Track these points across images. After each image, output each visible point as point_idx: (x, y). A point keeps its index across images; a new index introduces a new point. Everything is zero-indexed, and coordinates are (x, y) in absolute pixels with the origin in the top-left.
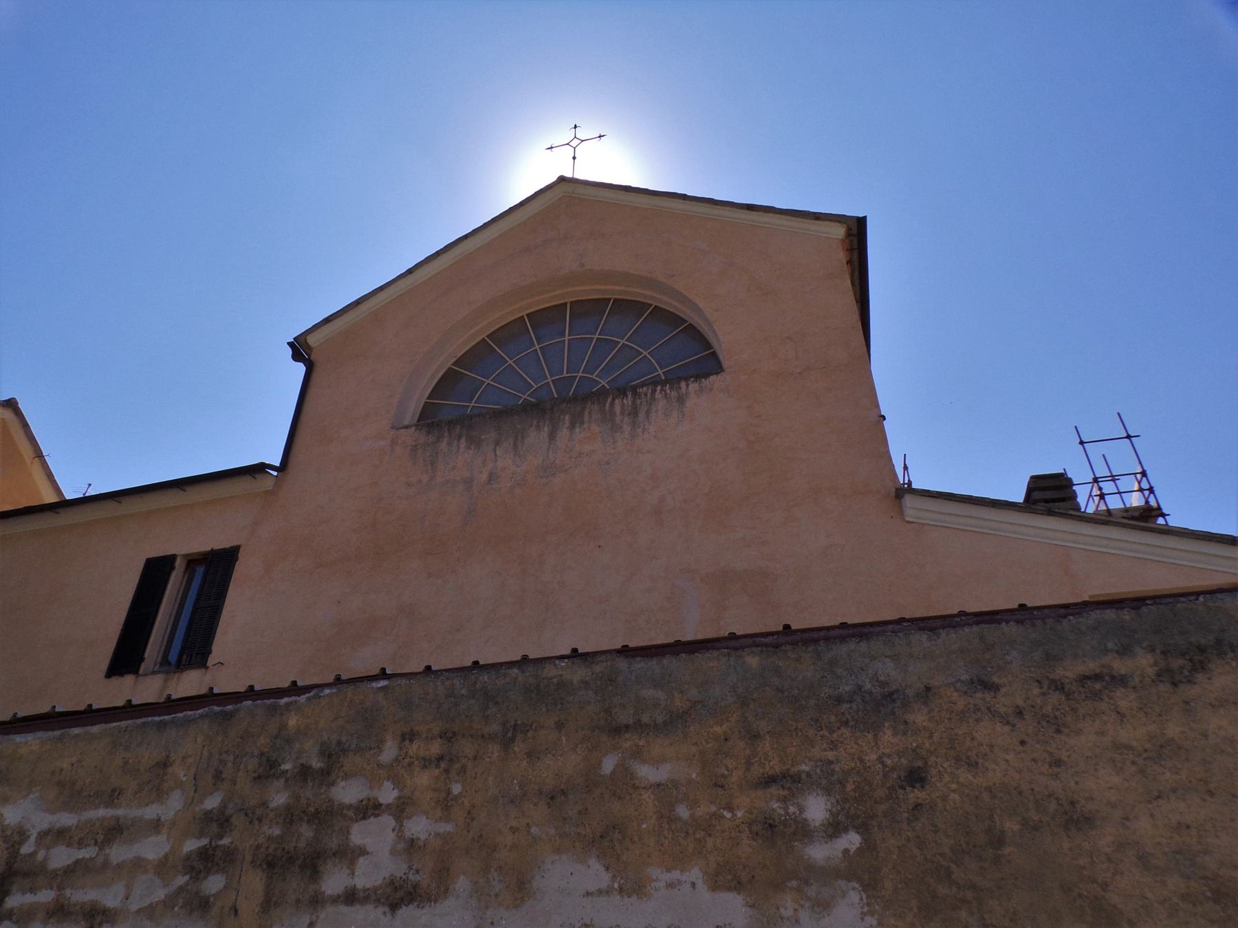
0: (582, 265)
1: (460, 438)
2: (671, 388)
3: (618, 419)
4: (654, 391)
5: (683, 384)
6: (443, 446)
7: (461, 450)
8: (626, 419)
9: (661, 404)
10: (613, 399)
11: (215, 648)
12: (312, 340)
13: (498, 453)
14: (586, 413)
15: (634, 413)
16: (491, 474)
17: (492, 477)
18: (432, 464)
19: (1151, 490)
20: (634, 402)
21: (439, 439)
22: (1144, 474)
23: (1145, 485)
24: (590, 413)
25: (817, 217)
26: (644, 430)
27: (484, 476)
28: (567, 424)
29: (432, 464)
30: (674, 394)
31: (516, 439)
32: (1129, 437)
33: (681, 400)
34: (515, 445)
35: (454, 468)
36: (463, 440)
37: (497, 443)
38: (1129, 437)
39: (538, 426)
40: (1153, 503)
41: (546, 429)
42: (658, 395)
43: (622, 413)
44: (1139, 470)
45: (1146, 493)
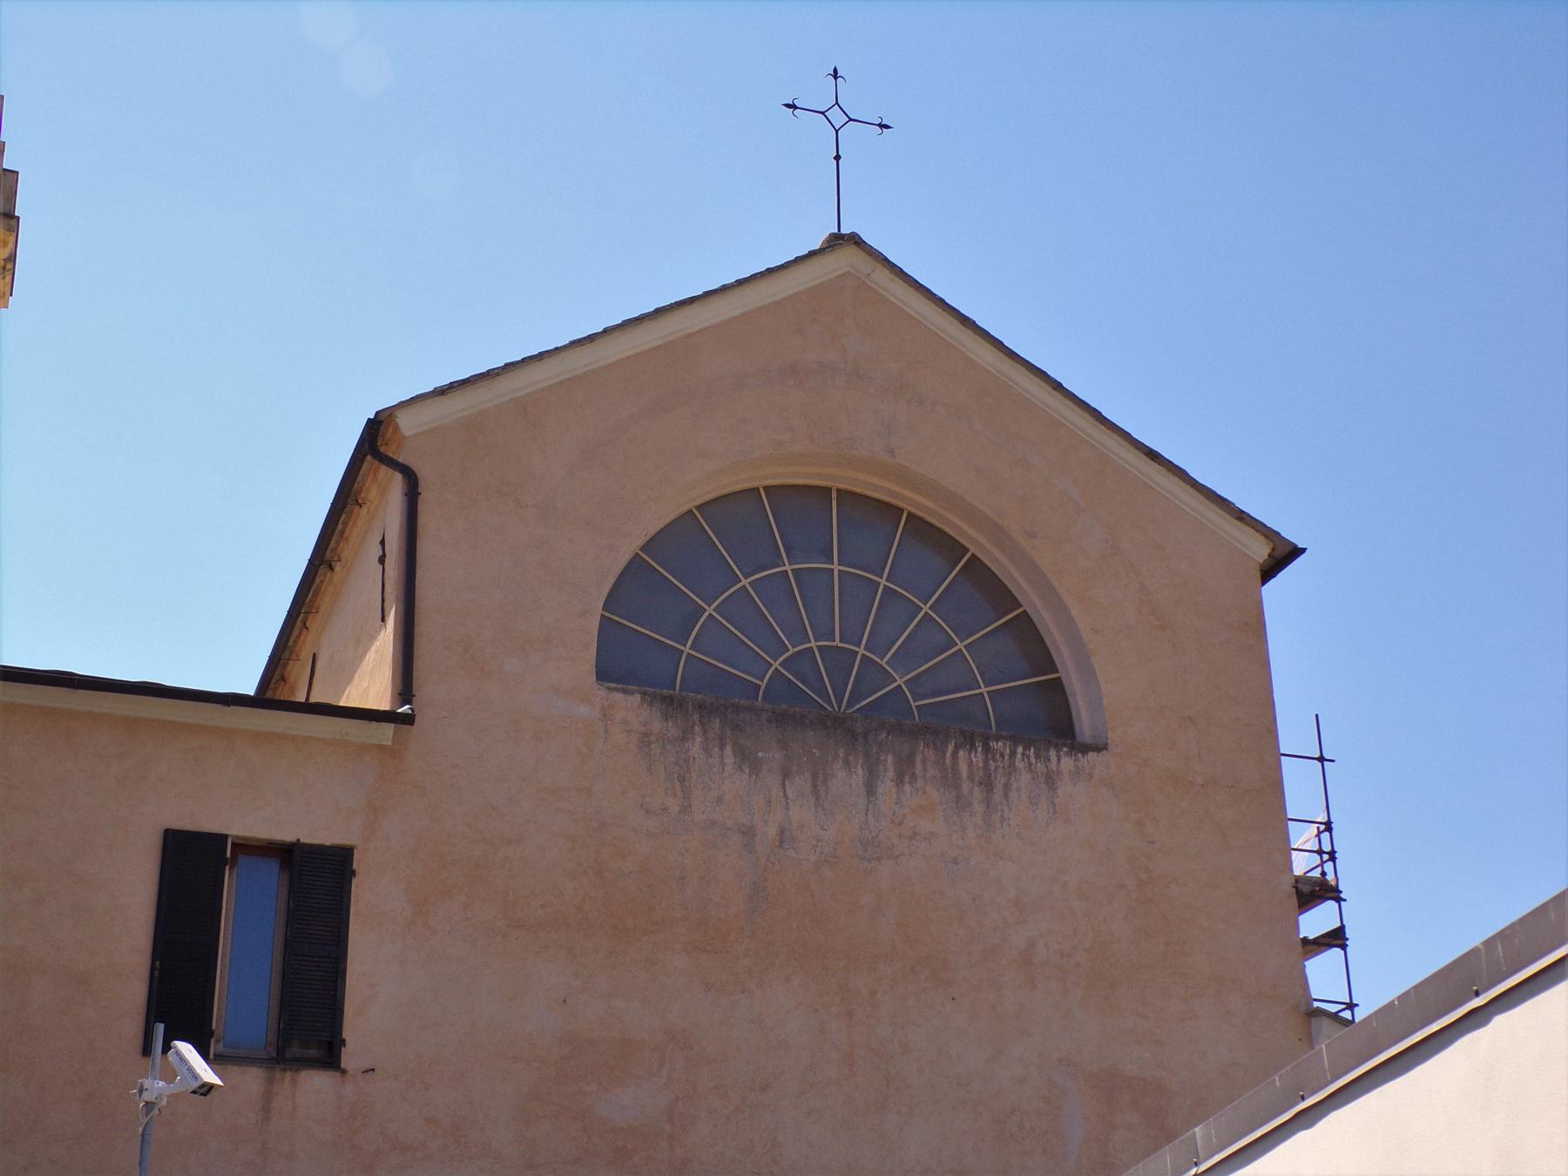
0: (891, 452)
1: (722, 747)
2: (1037, 756)
3: (965, 786)
4: (1013, 753)
5: (1053, 753)
6: (696, 747)
7: (729, 768)
8: (977, 792)
9: (1023, 779)
10: (957, 748)
11: (347, 1033)
12: (407, 424)
13: (789, 792)
14: (918, 759)
15: (987, 784)
16: (782, 832)
17: (784, 837)
18: (682, 780)
19: (1332, 856)
20: (986, 761)
21: (686, 735)
22: (1328, 826)
23: (1327, 848)
24: (924, 762)
25: (1242, 516)
26: (1003, 820)
27: (772, 831)
28: (891, 774)
29: (682, 780)
30: (1040, 767)
31: (815, 777)
32: (1321, 759)
33: (1051, 780)
34: (815, 787)
35: (720, 800)
36: (728, 749)
37: (786, 775)
38: (1321, 759)
39: (847, 763)
40: (1330, 877)
41: (860, 771)
42: (1020, 763)
43: (971, 777)
44: (1322, 818)
45: (1326, 857)
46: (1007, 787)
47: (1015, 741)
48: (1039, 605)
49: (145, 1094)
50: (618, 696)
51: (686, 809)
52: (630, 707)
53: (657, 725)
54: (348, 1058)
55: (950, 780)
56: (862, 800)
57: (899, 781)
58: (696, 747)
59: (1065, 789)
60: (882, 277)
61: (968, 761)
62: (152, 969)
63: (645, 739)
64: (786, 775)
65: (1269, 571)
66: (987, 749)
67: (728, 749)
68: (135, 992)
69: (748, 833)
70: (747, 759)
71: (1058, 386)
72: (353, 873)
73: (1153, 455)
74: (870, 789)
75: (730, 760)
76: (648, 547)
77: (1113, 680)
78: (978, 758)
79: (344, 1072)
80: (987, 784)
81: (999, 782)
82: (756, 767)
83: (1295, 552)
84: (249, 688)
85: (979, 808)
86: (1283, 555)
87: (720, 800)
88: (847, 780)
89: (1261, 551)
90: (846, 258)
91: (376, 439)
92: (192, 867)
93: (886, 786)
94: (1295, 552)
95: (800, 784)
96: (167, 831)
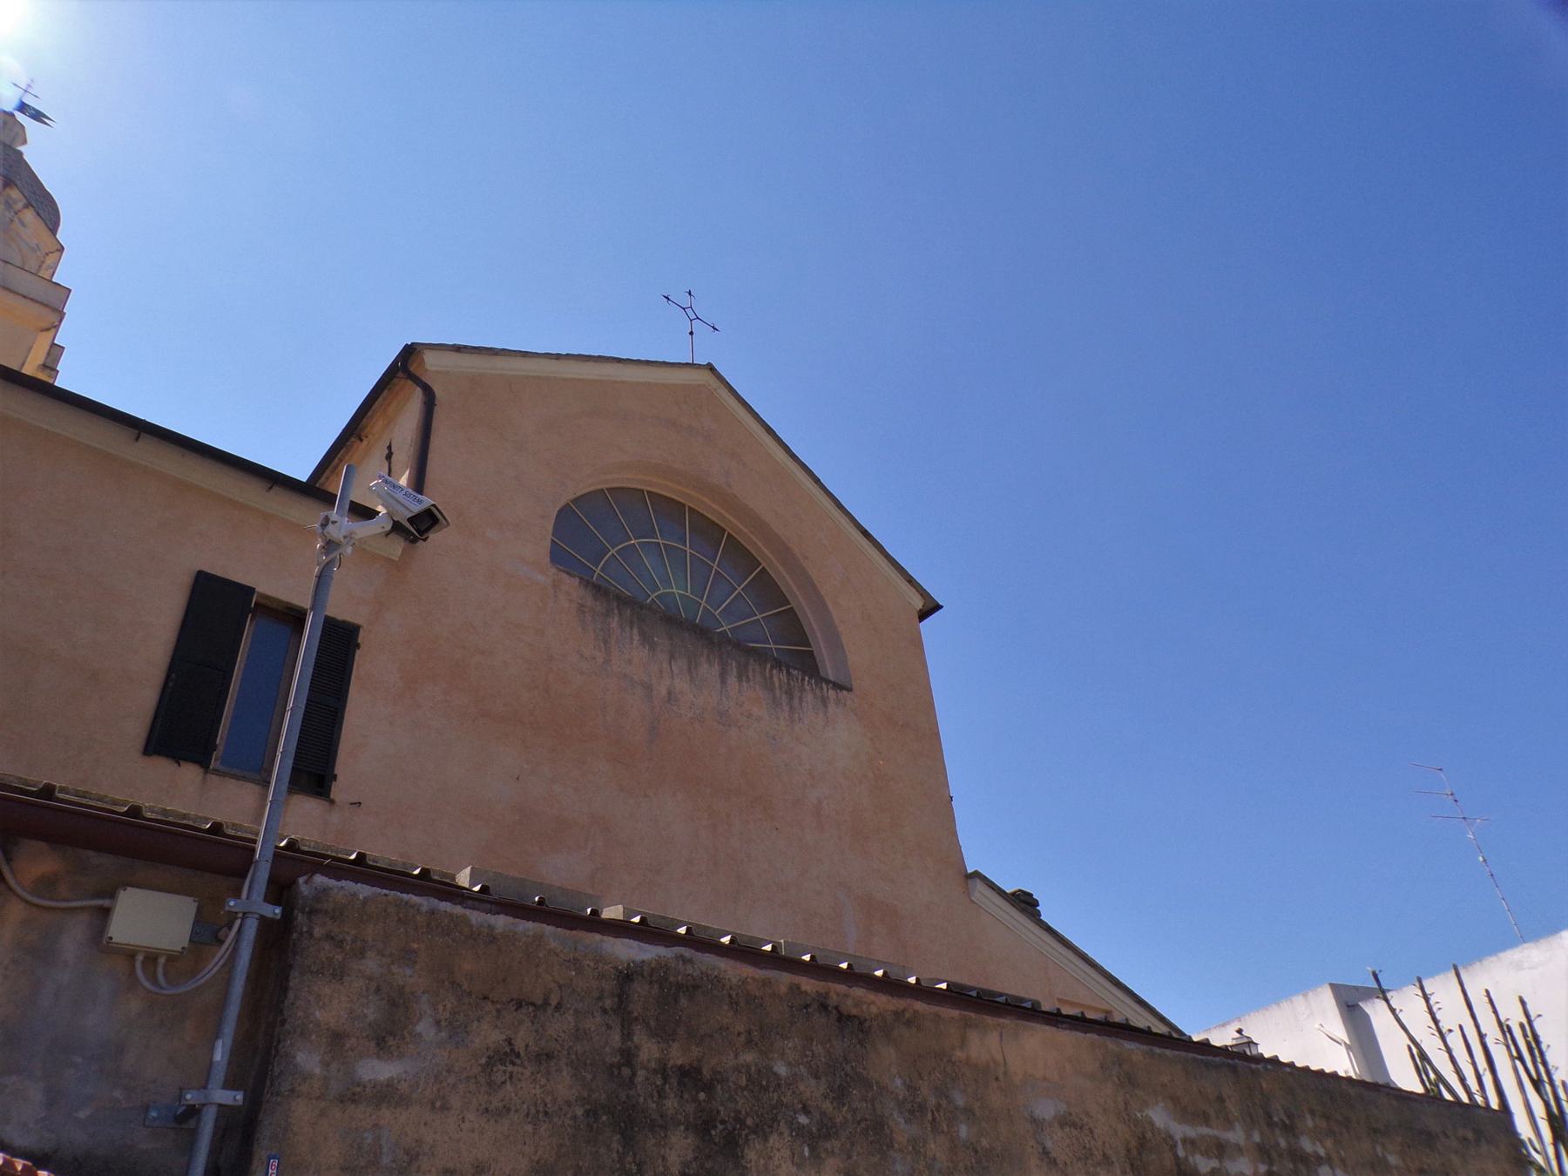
3: (778, 692)
9: (809, 697)
11: (341, 768)
12: (430, 359)
16: (670, 693)
18: (606, 642)
27: (664, 692)
33: (824, 701)
46: (801, 699)
47: (804, 673)
48: (804, 604)
49: (330, 527)
50: (565, 576)
51: (607, 661)
52: (571, 584)
53: (589, 601)
54: (335, 793)
55: (770, 688)
56: (718, 685)
57: (739, 678)
58: (614, 623)
59: (832, 708)
60: (724, 393)
61: (779, 677)
62: (168, 677)
63: (581, 608)
64: (672, 657)
65: (923, 615)
66: (788, 673)
67: (635, 631)
68: (146, 697)
69: (648, 688)
70: (646, 639)
71: (817, 481)
72: (358, 646)
73: (866, 533)
74: (723, 681)
75: (636, 637)
76: (575, 501)
77: (858, 650)
78: (784, 677)
79: (332, 802)
80: (790, 694)
81: (797, 694)
82: (653, 647)
83: (938, 607)
84: (303, 475)
85: (786, 708)
86: (931, 608)
87: (630, 661)
88: (709, 670)
89: (918, 603)
90: (706, 376)
91: (410, 353)
92: (216, 609)
93: (732, 680)
94: (938, 607)
95: (680, 665)
96: (200, 573)
